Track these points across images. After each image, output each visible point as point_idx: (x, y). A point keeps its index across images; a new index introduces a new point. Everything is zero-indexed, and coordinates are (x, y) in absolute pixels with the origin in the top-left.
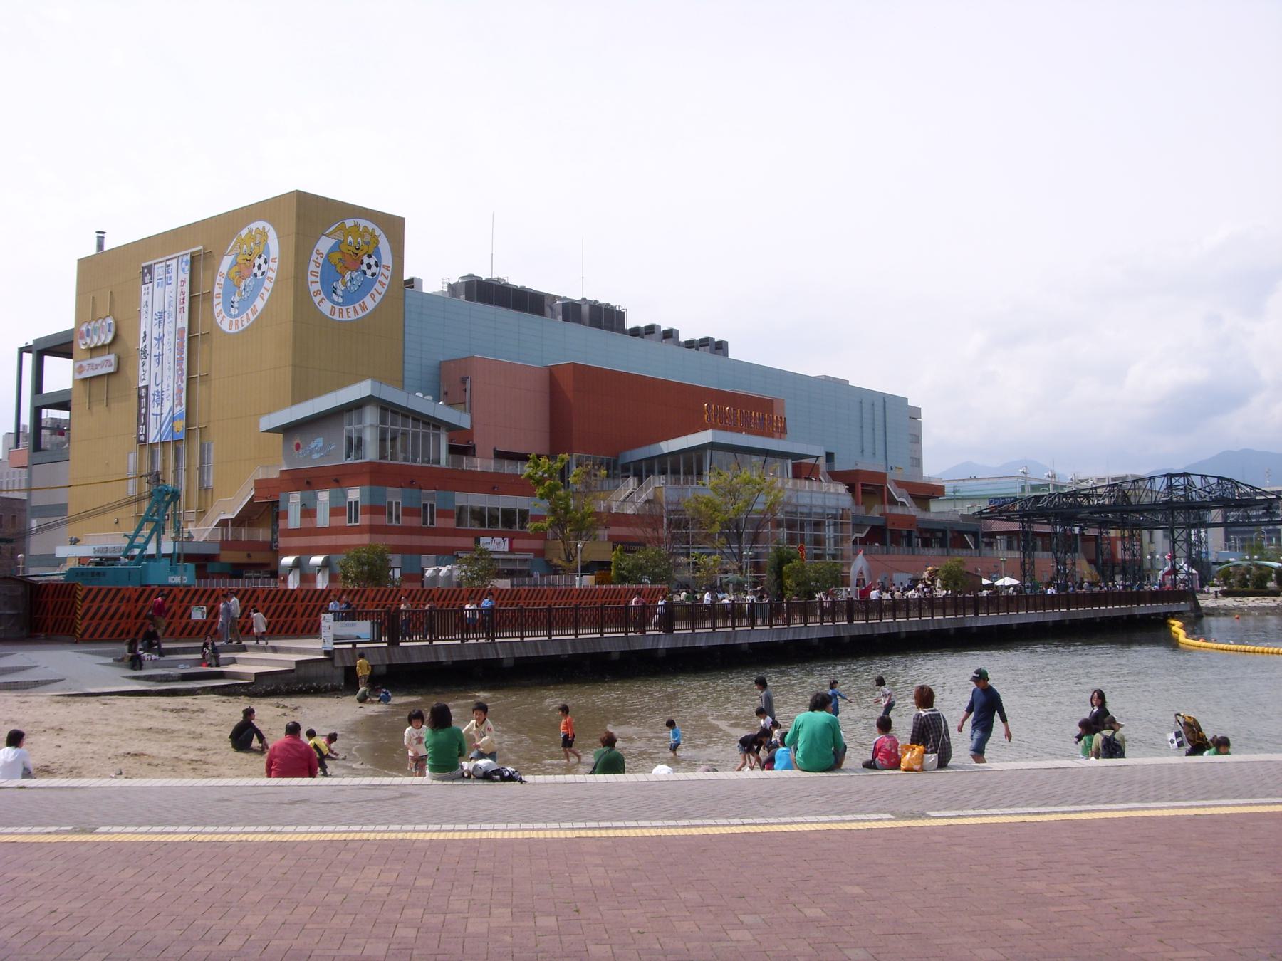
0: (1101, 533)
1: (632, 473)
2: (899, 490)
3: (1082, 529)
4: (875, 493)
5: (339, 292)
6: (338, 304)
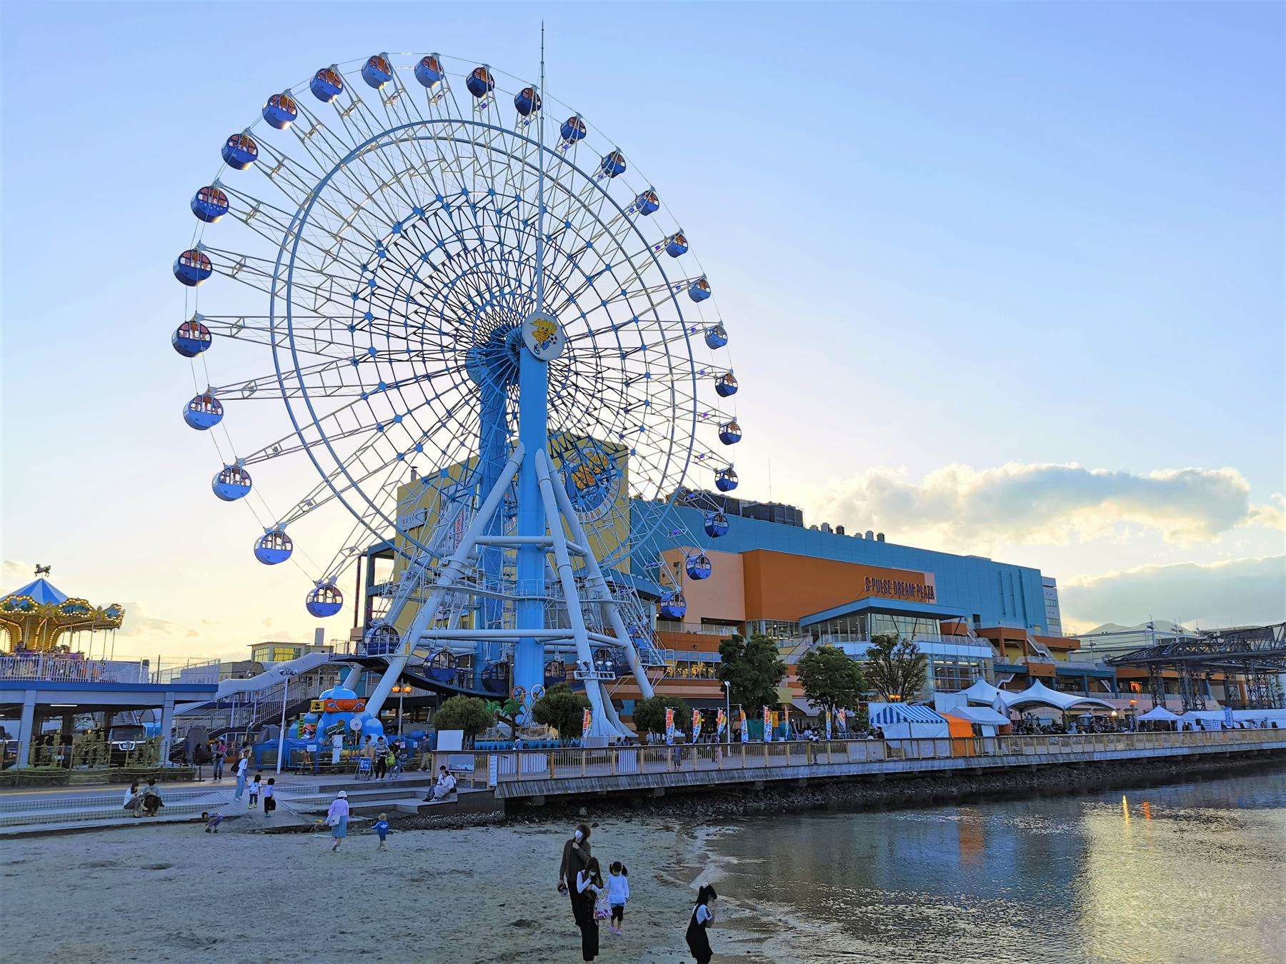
0: (1228, 678)
1: (810, 633)
2: (1037, 644)
3: (1208, 674)
4: (1018, 647)
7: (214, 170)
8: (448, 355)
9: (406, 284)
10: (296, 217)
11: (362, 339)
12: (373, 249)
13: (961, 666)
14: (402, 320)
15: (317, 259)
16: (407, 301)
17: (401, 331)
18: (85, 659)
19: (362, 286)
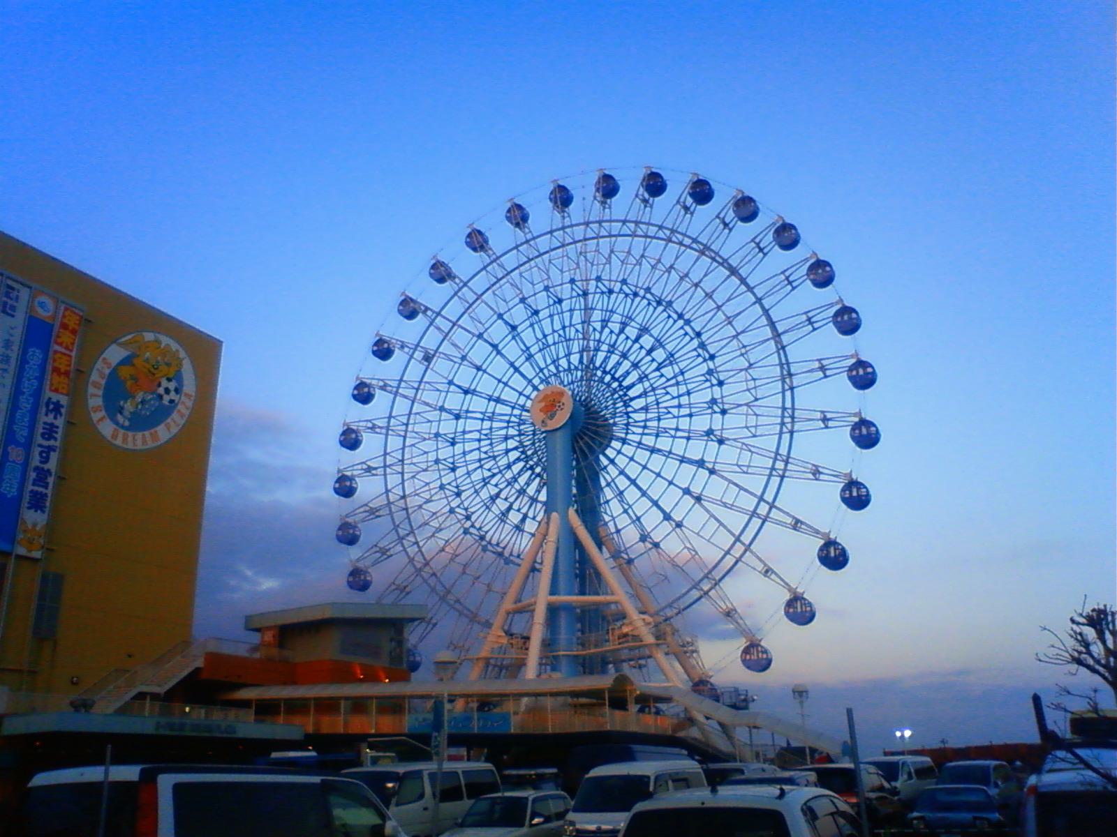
4: (515, 603)
5: (126, 413)
6: (123, 427)
7: (864, 344)
8: (552, 368)
9: (616, 318)
10: (717, 254)
11: (541, 301)
12: (640, 285)
13: (340, 703)
14: (567, 323)
15: (682, 266)
16: (602, 321)
17: (557, 326)
18: (30, 527)
19: (606, 283)
